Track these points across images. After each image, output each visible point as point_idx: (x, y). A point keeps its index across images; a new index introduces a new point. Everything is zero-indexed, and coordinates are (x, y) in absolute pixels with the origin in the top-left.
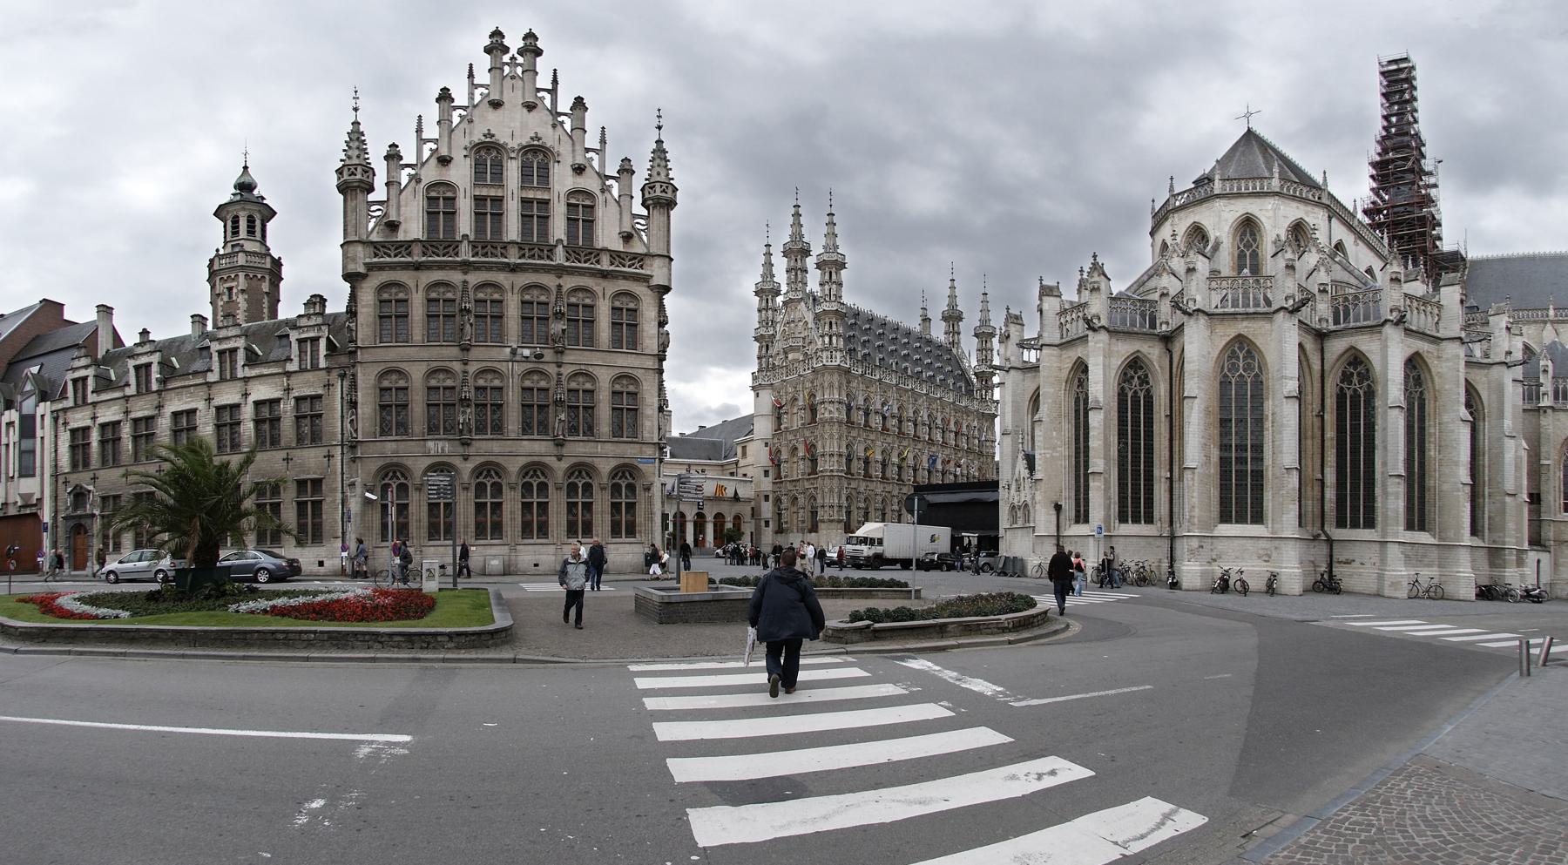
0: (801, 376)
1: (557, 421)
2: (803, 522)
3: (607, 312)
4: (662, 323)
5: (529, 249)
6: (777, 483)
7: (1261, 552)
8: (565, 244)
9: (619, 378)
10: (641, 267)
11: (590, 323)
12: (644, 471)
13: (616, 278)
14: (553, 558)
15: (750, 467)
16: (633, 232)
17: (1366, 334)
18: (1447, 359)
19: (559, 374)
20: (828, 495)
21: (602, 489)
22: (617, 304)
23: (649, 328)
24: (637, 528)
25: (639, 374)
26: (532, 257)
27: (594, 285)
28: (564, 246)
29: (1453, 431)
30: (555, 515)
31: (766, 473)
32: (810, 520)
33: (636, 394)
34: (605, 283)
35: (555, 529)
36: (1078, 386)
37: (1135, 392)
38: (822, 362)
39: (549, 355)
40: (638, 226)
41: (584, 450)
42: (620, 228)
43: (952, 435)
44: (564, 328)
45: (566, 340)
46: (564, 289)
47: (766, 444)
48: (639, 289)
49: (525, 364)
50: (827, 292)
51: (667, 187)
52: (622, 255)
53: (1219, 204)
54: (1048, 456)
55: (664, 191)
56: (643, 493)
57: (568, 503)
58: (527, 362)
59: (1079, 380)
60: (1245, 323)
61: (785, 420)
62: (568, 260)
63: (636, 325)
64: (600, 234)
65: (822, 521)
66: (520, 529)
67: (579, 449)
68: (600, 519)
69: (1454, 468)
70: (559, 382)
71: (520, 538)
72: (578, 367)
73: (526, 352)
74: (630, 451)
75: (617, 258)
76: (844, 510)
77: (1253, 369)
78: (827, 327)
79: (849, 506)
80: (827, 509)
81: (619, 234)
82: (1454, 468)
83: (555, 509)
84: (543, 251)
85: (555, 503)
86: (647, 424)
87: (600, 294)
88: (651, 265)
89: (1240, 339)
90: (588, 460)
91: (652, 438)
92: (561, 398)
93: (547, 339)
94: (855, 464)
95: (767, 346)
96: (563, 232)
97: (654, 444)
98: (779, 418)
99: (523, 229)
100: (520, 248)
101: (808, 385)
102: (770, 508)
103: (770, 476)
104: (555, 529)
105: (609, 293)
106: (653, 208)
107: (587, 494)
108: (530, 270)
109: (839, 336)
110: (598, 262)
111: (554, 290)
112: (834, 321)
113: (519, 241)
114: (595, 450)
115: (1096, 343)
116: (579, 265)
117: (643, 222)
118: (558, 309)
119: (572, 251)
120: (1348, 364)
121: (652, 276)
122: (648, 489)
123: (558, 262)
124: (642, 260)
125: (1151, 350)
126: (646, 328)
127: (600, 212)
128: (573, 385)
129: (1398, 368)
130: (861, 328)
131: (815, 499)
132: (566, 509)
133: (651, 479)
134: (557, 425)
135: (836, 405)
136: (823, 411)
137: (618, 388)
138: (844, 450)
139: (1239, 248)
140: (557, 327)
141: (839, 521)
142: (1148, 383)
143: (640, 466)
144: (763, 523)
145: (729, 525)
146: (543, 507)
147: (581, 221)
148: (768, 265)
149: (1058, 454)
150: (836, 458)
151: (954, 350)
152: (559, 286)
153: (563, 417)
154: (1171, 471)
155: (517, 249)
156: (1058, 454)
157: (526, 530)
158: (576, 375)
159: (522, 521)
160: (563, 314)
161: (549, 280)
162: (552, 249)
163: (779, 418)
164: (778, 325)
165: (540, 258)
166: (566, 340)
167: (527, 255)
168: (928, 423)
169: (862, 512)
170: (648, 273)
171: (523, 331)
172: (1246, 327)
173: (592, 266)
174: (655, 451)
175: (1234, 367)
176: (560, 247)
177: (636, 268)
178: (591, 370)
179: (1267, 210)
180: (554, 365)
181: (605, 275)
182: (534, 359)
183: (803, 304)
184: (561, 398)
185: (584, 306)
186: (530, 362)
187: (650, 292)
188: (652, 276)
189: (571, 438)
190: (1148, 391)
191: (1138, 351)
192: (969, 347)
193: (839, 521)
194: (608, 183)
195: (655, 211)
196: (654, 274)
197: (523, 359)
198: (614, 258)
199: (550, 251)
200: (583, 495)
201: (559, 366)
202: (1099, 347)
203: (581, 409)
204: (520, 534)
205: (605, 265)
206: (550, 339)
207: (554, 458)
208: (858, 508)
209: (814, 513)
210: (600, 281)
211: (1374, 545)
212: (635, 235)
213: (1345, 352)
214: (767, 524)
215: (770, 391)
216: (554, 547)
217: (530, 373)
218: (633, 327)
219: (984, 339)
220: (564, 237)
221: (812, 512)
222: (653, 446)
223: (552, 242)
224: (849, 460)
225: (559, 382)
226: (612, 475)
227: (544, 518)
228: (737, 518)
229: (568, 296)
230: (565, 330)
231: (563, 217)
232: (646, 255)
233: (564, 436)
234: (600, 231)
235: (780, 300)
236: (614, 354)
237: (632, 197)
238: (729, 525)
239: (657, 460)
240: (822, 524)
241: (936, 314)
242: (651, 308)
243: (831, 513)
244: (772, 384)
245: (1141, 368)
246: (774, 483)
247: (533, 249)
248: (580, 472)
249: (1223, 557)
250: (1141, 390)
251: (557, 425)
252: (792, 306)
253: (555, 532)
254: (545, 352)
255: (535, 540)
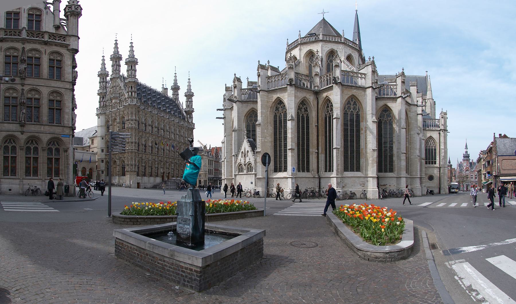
0: (118, 109)
1: (21, 113)
2: (119, 172)
3: (47, 61)
4: (75, 67)
5: (9, 32)
6: (107, 155)
7: (361, 183)
8: (27, 29)
9: (53, 92)
10: (64, 41)
11: (38, 65)
12: (64, 141)
13: (52, 45)
14: (18, 186)
15: (95, 148)
16: (60, 26)
17: (391, 100)
18: (412, 112)
19: (23, 90)
20: (130, 160)
21: (43, 150)
22: (52, 57)
23: (67, 69)
24: (60, 172)
25: (62, 91)
26: (11, 35)
27: (40, 48)
28: (26, 30)
29: (414, 137)
30: (20, 164)
31: (102, 151)
32: (122, 171)
33: (61, 101)
34: (46, 47)
35: (19, 170)
36: (276, 110)
37: (303, 115)
38: (128, 103)
39: (18, 80)
40: (62, 23)
41: (34, 129)
42: (54, 23)
43: (178, 136)
44: (25, 67)
45: (26, 73)
46: (26, 50)
47: (103, 139)
48: (63, 51)
49: (6, 85)
50: (130, 74)
51: (78, 7)
52: (55, 35)
53: (320, 44)
54: (263, 141)
55: (76, 9)
56: (63, 153)
57: (26, 157)
58: (8, 83)
59: (276, 107)
60: (355, 91)
61: (111, 128)
62: (28, 36)
63: (61, 68)
64: (44, 26)
65: (128, 171)
66: (3, 170)
67: (32, 128)
68: (42, 166)
69: (415, 150)
70: (22, 93)
71: (2, 175)
72: (32, 87)
73: (7, 79)
74: (58, 130)
75: (52, 36)
76: (137, 167)
77: (356, 109)
78: (130, 88)
79: (138, 165)
80: (130, 166)
81: (53, 26)
82: (415, 150)
83: (20, 160)
84: (16, 32)
85: (20, 157)
86: (66, 117)
87: (44, 52)
88: (69, 40)
89: (353, 97)
90: (36, 134)
91: (69, 124)
92: (23, 101)
93: (17, 73)
94: (141, 147)
95: (103, 97)
96: (26, 24)
97: (70, 127)
98: (108, 128)
99: (6, 24)
100: (6, 32)
101: (122, 113)
102: (104, 166)
103: (104, 152)
104: (19, 170)
105: (48, 52)
106: (70, 16)
107: (35, 153)
108: (10, 41)
109: (135, 92)
110: (43, 37)
111: (21, 50)
112: (133, 86)
113: (5, 28)
114: (40, 129)
115: (291, 91)
116: (33, 38)
117: (65, 22)
118: (23, 58)
119: (30, 32)
120: (278, 104)
121: (69, 45)
122: (66, 151)
123: (23, 37)
124: (65, 37)
125: (310, 97)
126: (66, 69)
127: (44, 17)
128: (30, 96)
129: (404, 114)
130: (142, 90)
131: (124, 162)
132: (25, 161)
133: (68, 146)
134: (21, 115)
135: (134, 121)
136: (128, 124)
137: (51, 98)
138: (137, 141)
139: (309, 63)
140: (22, 67)
141: (135, 171)
142: (307, 111)
143: (63, 138)
144: (101, 172)
145: (88, 172)
146: (14, 159)
147: (34, 21)
148: (104, 64)
149: (267, 140)
150: (134, 144)
151: (176, 102)
152: (24, 48)
153: (24, 111)
154: (318, 149)
155: (4, 32)
156: (267, 140)
157: (28, 172)
158: (31, 90)
159: (4, 166)
160: (25, 61)
161: (19, 46)
162: (20, 32)
163: (108, 128)
164: (108, 89)
165: (14, 35)
166: (26, 73)
167: (8, 34)
168: (169, 131)
169: (144, 167)
170: (68, 43)
171: (5, 69)
172: (355, 92)
173: (40, 39)
174: (70, 131)
175: (349, 108)
176: (24, 31)
177: (61, 41)
178: (38, 88)
179: (340, 49)
180: (20, 85)
181: (46, 43)
182: (11, 82)
183: (119, 79)
184: (23, 101)
185: (35, 58)
186: (9, 84)
187: (68, 52)
188: (69, 45)
189: (28, 123)
190: (307, 115)
191: (305, 97)
192: (182, 100)
193: (135, 171)
194: (48, 5)
195: (71, 18)
196: (70, 44)
197: (5, 82)
198: (51, 36)
199: (20, 32)
200: (33, 153)
201: (23, 86)
202: (293, 93)
203: (33, 108)
204: (3, 173)
205: (46, 38)
206: (18, 73)
207: (20, 133)
208: (142, 166)
209: (124, 168)
210: (44, 46)
211: (394, 178)
212: (61, 27)
213: (382, 106)
214: (103, 172)
215: (105, 116)
216: (19, 180)
217: (8, 89)
218: (60, 68)
219: (189, 97)
220: (26, 27)
221: (123, 167)
222: (69, 128)
223: (20, 28)
224: (139, 145)
225: (22, 93)
226: (48, 143)
227: (14, 165)
228: (91, 169)
229: (28, 53)
230: (26, 68)
231: (26, 18)
232: (66, 35)
233: (25, 121)
234: (44, 24)
235: (108, 78)
236: (50, 81)
237: (60, 11)
238: (88, 172)
239: (71, 136)
240: (128, 173)
241: (169, 88)
242: (69, 60)
243: (132, 168)
244: (105, 113)
245: (305, 104)
246: (106, 155)
247: (11, 32)
248: (32, 141)
249: (347, 185)
250: (282, 112)
251: (21, 115)
252: (114, 80)
253: (20, 172)
254: (16, 78)
255: (10, 177)
